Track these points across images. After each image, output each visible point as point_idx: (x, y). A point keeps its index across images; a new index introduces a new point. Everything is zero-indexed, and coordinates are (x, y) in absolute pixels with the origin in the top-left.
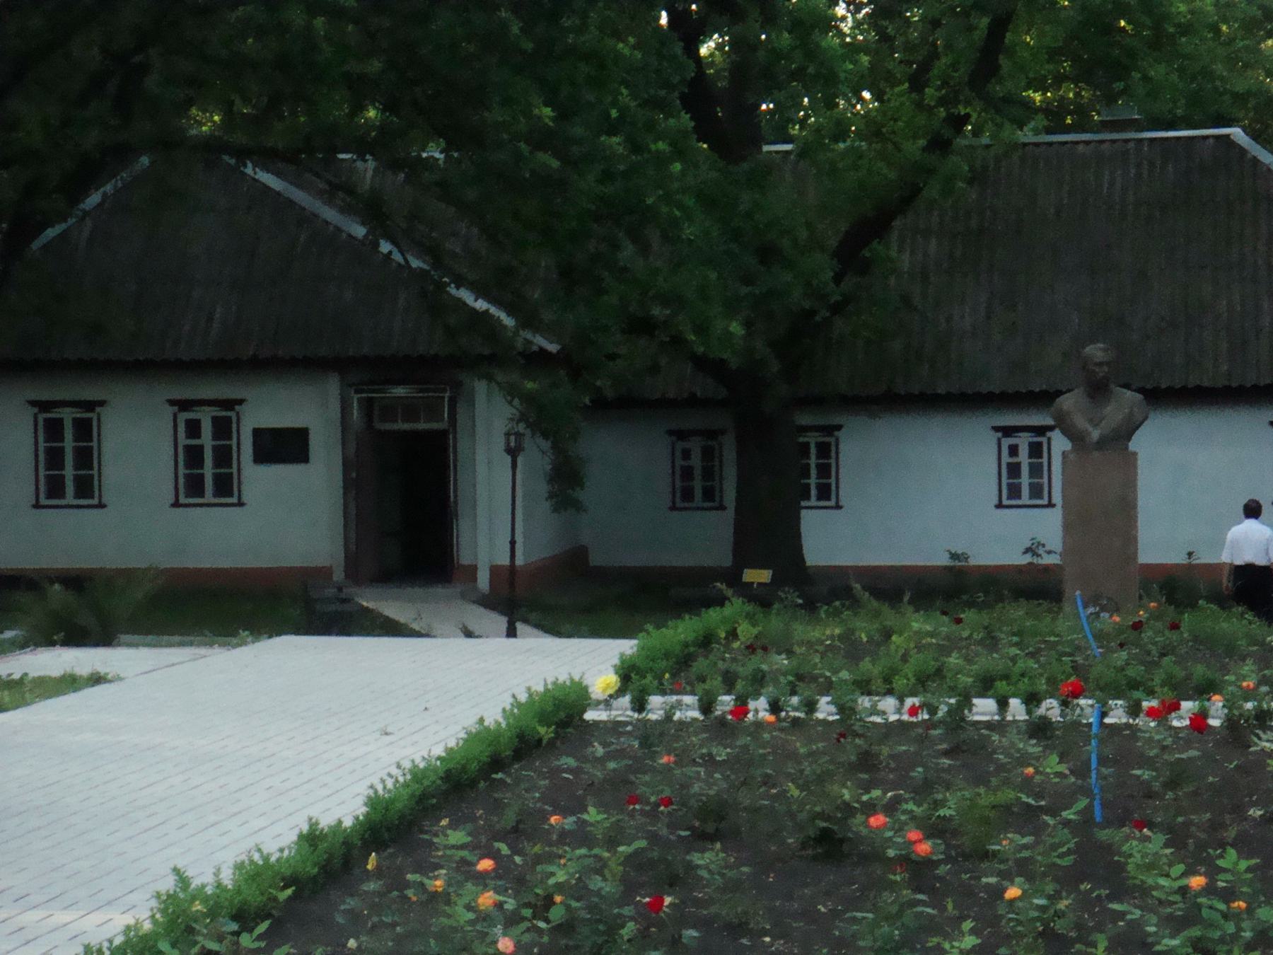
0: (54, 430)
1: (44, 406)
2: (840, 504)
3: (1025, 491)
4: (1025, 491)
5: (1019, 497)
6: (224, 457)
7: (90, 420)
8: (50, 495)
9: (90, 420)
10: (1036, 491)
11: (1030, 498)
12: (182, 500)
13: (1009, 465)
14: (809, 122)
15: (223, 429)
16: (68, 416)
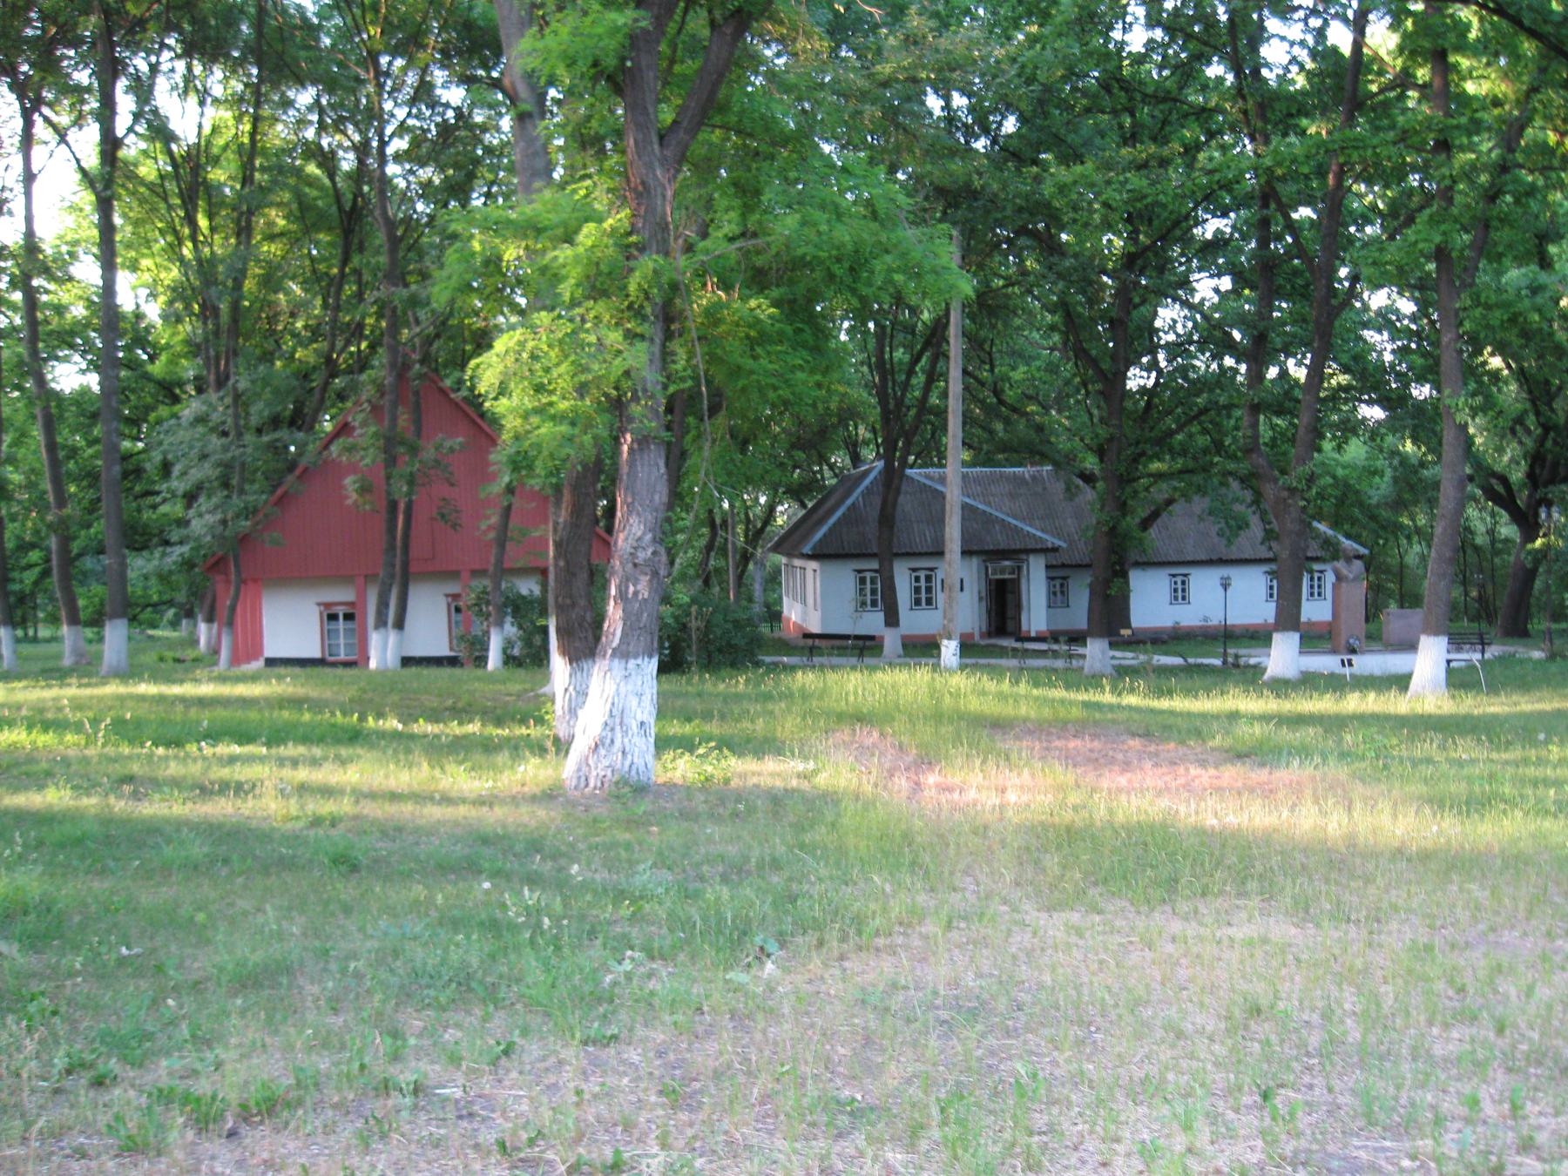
0: (863, 581)
1: (859, 571)
6: (929, 590)
10: (1184, 598)
15: (928, 578)
16: (868, 575)
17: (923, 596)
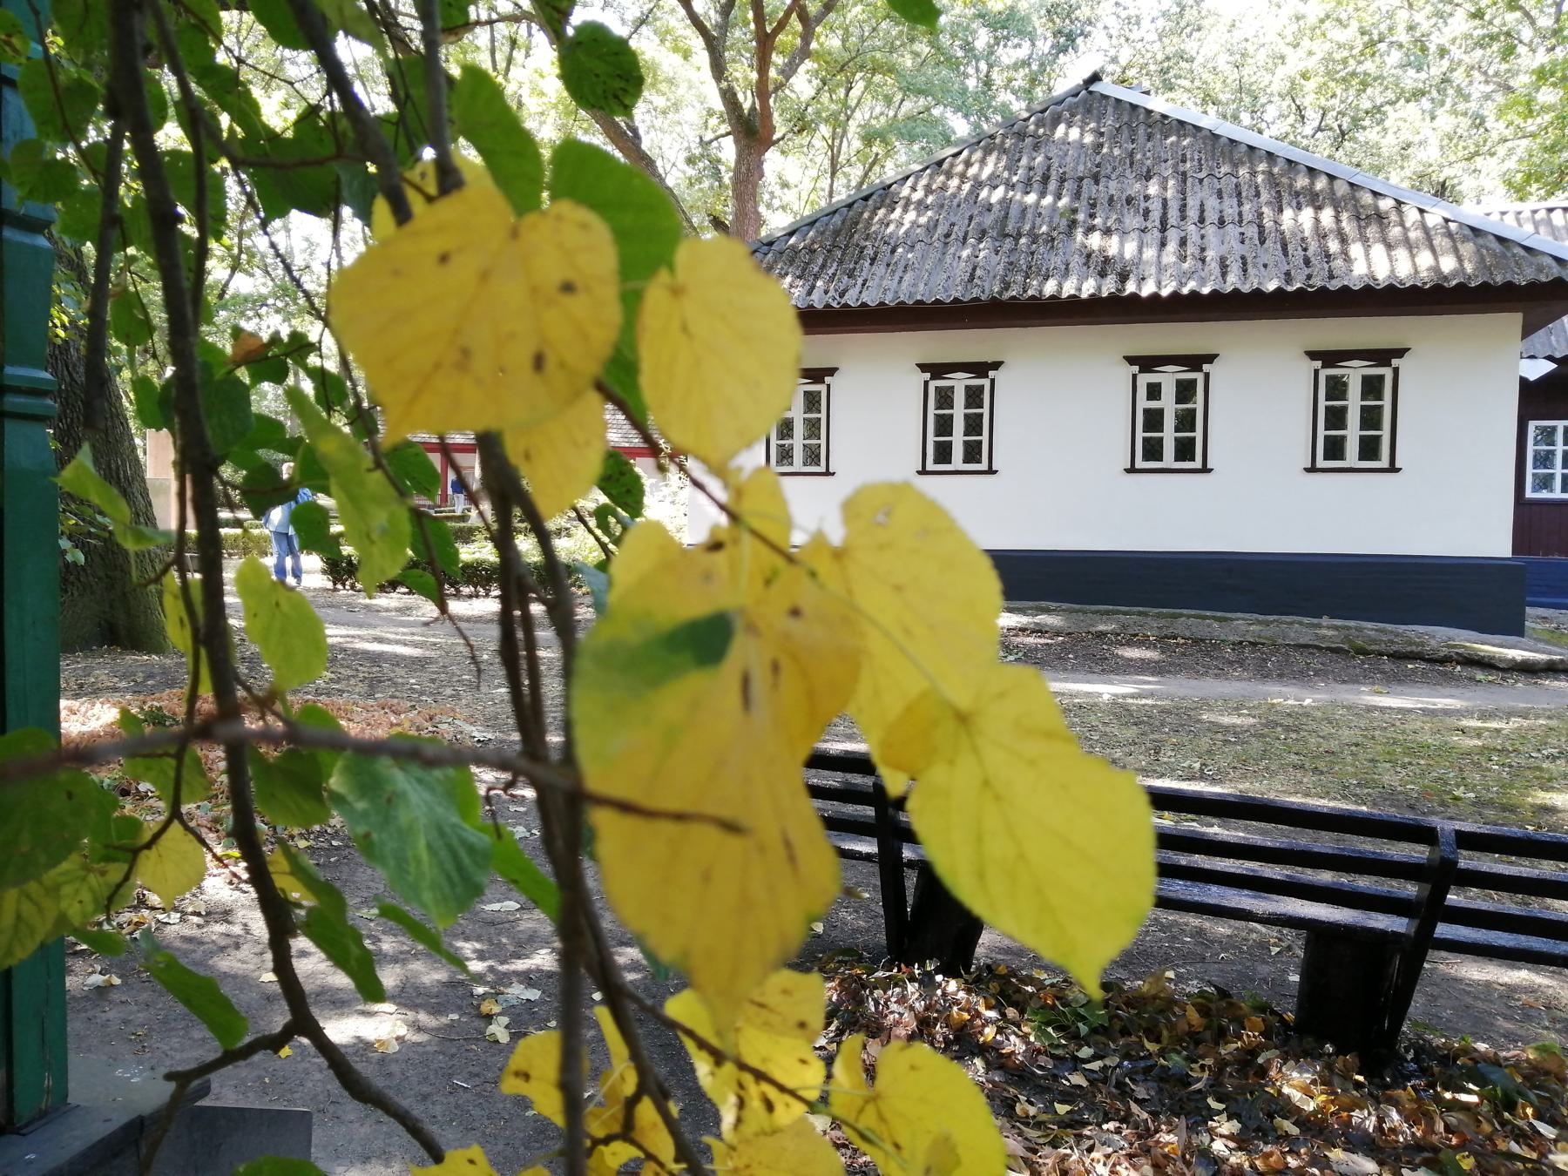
2: (1398, 465)
3: (1169, 449)
4: (1169, 449)
5: (1161, 459)
7: (1381, 378)
8: (1146, 458)
9: (1381, 378)
10: (972, 453)
11: (1177, 459)
12: (930, 466)
13: (1147, 412)
14: (368, 164)
17: (958, 439)
